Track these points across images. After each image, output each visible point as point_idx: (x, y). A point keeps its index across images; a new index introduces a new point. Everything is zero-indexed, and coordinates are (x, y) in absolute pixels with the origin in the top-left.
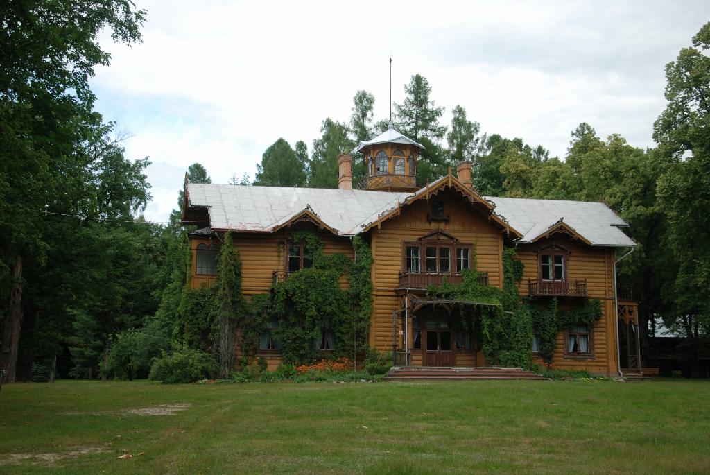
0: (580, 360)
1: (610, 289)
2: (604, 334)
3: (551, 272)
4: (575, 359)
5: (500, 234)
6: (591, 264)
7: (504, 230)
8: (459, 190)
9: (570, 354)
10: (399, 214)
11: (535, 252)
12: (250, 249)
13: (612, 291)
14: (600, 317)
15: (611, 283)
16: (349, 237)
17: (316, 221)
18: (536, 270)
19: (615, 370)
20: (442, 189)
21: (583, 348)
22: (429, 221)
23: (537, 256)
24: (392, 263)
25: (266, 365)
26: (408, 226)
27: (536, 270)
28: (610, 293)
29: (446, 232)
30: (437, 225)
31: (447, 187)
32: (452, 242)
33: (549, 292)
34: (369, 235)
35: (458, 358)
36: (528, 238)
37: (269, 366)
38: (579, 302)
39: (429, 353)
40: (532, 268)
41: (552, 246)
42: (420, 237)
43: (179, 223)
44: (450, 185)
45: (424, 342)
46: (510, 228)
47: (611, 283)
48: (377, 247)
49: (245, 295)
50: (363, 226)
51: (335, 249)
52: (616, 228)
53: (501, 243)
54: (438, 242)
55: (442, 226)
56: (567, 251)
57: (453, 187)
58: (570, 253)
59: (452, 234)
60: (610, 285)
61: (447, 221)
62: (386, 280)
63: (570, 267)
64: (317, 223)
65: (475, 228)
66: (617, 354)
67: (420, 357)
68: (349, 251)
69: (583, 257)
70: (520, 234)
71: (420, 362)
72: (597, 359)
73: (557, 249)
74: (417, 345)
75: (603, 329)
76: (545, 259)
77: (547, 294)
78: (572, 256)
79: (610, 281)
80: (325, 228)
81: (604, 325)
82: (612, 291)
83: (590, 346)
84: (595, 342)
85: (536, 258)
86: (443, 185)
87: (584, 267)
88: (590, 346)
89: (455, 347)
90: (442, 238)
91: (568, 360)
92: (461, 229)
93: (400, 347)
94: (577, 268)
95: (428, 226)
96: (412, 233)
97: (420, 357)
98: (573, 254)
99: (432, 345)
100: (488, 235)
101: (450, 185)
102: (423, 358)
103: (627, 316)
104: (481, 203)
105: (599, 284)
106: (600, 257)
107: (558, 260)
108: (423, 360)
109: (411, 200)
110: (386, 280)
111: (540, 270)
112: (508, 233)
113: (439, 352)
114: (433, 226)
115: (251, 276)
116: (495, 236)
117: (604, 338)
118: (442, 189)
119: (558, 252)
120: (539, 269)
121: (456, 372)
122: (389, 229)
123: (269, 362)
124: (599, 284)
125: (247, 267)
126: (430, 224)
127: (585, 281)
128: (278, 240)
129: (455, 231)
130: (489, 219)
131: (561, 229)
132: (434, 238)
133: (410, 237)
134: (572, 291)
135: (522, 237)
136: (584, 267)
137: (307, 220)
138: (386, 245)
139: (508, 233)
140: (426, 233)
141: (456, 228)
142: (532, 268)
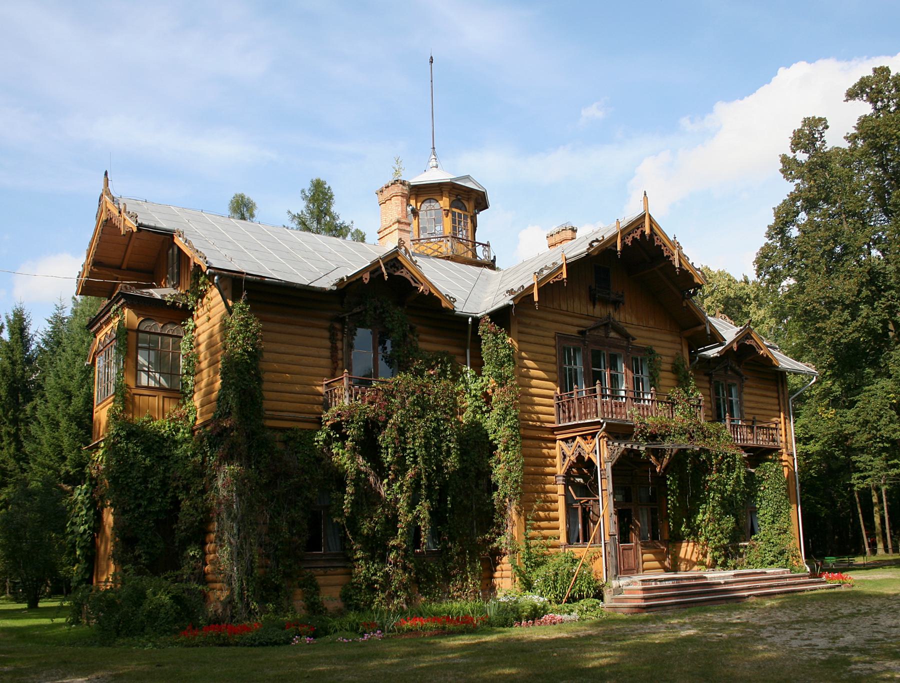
7: (700, 328)
10: (565, 276)
11: (706, 375)
14: (128, 422)
23: (710, 382)
25: (317, 588)
37: (322, 589)
41: (726, 367)
42: (581, 329)
43: (144, 564)
49: (271, 428)
61: (616, 304)
63: (746, 404)
65: (651, 323)
69: (767, 390)
87: (760, 405)
90: (613, 334)
96: (569, 320)
100: (669, 338)
114: (599, 311)
116: (678, 340)
121: (720, 584)
123: (320, 580)
125: (272, 376)
132: (601, 333)
133: (565, 327)
136: (760, 405)
138: (532, 339)
140: (589, 323)
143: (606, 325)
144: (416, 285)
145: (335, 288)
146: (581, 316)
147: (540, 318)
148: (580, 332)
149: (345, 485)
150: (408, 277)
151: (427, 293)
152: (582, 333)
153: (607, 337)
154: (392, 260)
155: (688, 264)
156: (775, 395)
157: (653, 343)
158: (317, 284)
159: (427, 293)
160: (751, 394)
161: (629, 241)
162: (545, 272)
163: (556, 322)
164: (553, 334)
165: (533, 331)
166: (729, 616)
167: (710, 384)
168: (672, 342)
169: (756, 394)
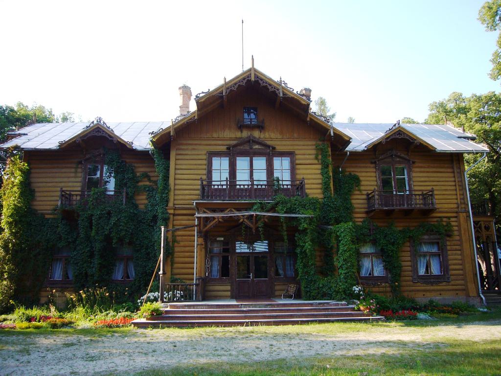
1: (462, 201)
4: (427, 283)
6: (439, 175)
8: (273, 90)
11: (372, 163)
13: (464, 203)
15: (463, 195)
16: (148, 151)
17: (109, 135)
18: (375, 183)
19: (476, 295)
23: (375, 167)
26: (215, 135)
27: (375, 183)
28: (463, 206)
32: (268, 150)
34: (166, 142)
35: (277, 288)
36: (359, 142)
40: (369, 179)
41: (392, 156)
44: (253, 79)
46: (334, 129)
48: (177, 154)
50: (152, 133)
55: (256, 134)
56: (409, 160)
58: (414, 163)
59: (269, 143)
60: (462, 197)
63: (414, 179)
66: (476, 274)
67: (229, 288)
69: (428, 167)
70: (347, 136)
71: (229, 293)
72: (453, 283)
78: (417, 167)
79: (461, 193)
82: (464, 203)
84: (450, 262)
85: (374, 170)
86: (244, 79)
90: (257, 147)
91: (419, 284)
92: (279, 136)
94: (422, 179)
95: (239, 134)
98: (417, 165)
101: (253, 79)
103: (484, 233)
106: (448, 168)
108: (232, 291)
109: (202, 97)
112: (332, 134)
114: (245, 134)
115: (49, 194)
119: (399, 163)
122: (200, 139)
126: (242, 132)
127: (432, 191)
129: (272, 139)
131: (399, 134)
132: (247, 147)
134: (418, 203)
139: (332, 134)
140: (235, 142)
141: (273, 135)
142: (369, 179)
143: (249, 141)
144: (111, 139)
145: (366, 149)
147: (196, 144)
153: (251, 149)
155: (294, 94)
160: (417, 172)
163: (210, 145)
164: (205, 152)
165: (189, 153)
169: (427, 172)
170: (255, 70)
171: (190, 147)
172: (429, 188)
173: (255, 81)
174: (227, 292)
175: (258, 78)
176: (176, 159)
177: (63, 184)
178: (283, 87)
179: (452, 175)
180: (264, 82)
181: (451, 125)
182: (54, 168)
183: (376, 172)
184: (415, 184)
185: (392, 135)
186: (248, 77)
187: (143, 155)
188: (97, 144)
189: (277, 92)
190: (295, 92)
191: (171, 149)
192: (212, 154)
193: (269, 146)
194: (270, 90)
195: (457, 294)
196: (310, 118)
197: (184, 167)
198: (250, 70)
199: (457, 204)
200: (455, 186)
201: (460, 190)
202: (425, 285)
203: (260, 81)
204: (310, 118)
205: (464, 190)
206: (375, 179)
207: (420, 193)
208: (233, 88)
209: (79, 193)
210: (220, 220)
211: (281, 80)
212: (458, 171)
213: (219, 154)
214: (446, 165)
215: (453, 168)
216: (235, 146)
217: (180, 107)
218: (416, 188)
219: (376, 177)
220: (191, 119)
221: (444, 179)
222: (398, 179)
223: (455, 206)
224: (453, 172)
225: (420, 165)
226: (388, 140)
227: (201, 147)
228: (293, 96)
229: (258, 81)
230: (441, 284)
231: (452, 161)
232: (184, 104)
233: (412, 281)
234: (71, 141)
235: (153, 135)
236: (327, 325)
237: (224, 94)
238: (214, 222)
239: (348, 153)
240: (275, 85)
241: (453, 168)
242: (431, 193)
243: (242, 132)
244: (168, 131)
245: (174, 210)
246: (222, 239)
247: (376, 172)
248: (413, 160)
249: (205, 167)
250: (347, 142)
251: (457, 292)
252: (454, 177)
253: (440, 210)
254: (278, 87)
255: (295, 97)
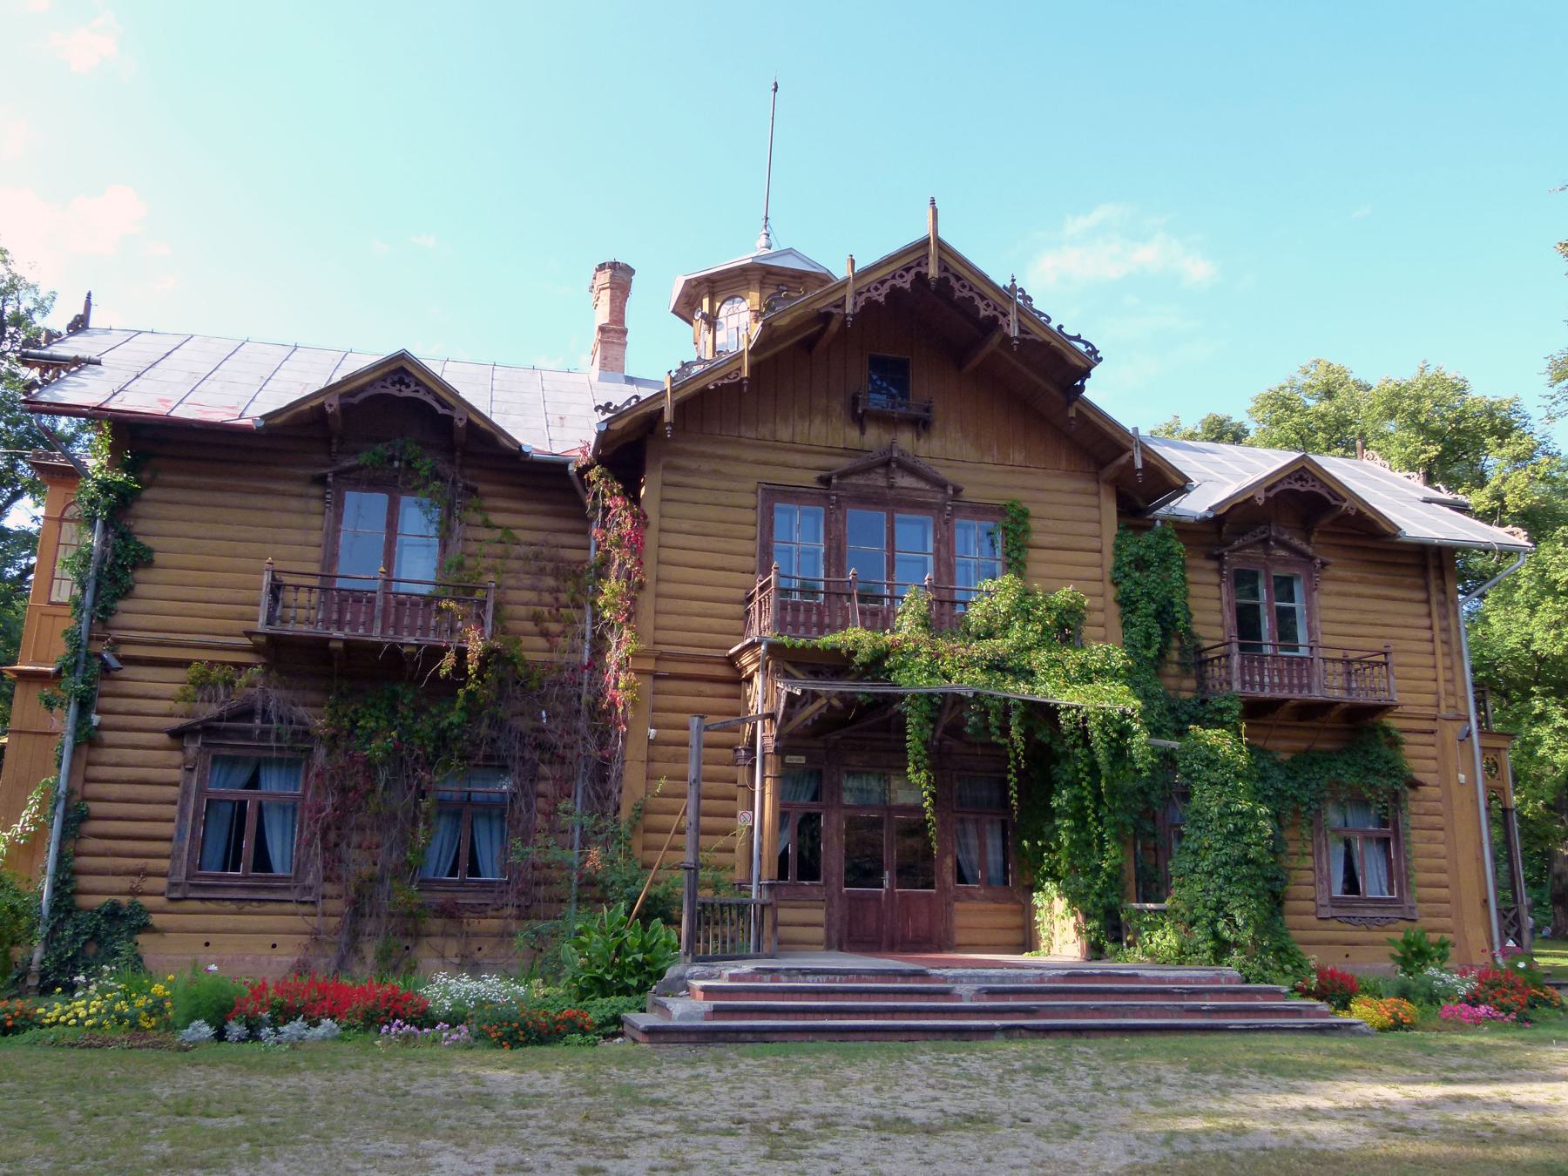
0: (1368, 924)
2: (1440, 834)
3: (1266, 625)
5: (1105, 481)
7: (1124, 459)
8: (966, 293)
9: (1334, 902)
10: (746, 374)
11: (1210, 557)
12: (196, 496)
15: (1451, 668)
16: (565, 465)
17: (439, 400)
20: (906, 283)
21: (1373, 881)
22: (859, 420)
23: (1219, 571)
24: (718, 560)
26: (784, 434)
27: (1218, 618)
29: (924, 463)
30: (887, 438)
31: (921, 278)
33: (1272, 686)
38: (1359, 728)
39: (851, 898)
41: (1265, 541)
42: (823, 473)
44: (933, 271)
45: (833, 856)
46: (1146, 450)
47: (1451, 668)
50: (606, 408)
51: (529, 513)
52: (1446, 510)
53: (1110, 508)
54: (890, 494)
55: (905, 440)
56: (1312, 559)
57: (943, 282)
58: (1324, 564)
59: (945, 474)
61: (921, 425)
62: (697, 622)
64: (444, 404)
65: (1018, 457)
67: (819, 915)
68: (572, 524)
69: (1361, 581)
71: (820, 933)
73: (1282, 553)
74: (798, 864)
75: (1436, 819)
76: (1244, 580)
77: (1267, 693)
80: (469, 421)
81: (1437, 792)
83: (1396, 874)
85: (1215, 579)
87: (1370, 617)
88: (1396, 874)
89: (949, 878)
90: (904, 481)
91: (1334, 923)
92: (970, 453)
93: (739, 875)
94: (1345, 616)
95: (852, 436)
97: (819, 915)
99: (863, 871)
101: (933, 271)
102: (828, 915)
104: (1045, 344)
105: (1416, 673)
107: (1284, 588)
108: (829, 926)
110: (697, 622)
111: (1230, 620)
112: (1139, 465)
113: (890, 893)
114: (874, 438)
116: (1092, 486)
117: (1442, 849)
118: (906, 283)
119: (1286, 562)
120: (1228, 615)
124: (1416, 673)
126: (863, 432)
128: (310, 471)
130: (1072, 413)
131: (1301, 478)
134: (1329, 687)
135: (1181, 485)
137: (407, 393)
138: (699, 496)
139: (1139, 465)
140: (843, 463)
143: (886, 464)
144: (446, 412)
145: (1211, 515)
146: (830, 451)
147: (723, 458)
148: (821, 480)
149: (933, 805)
150: (1323, 492)
151: (1353, 513)
152: (825, 481)
153: (891, 487)
154: (395, 372)
155: (1049, 331)
156: (1421, 595)
157: (1018, 495)
158: (183, 413)
159: (1353, 513)
161: (861, 301)
162: (696, 369)
163: (765, 463)
164: (752, 485)
166: (837, 1087)
167: (1221, 575)
168: (1074, 492)
169: (1358, 596)
170: (941, 246)
171: (705, 466)
172: (1379, 645)
173: (940, 279)
174: (813, 929)
175: (946, 269)
176: (663, 500)
177: (281, 550)
178: (1020, 309)
179: (1423, 609)
180: (964, 286)
181: (1379, 460)
182: (220, 489)
183: (1219, 586)
184: (1327, 627)
185: (1281, 481)
186: (919, 265)
187: (548, 481)
188: (392, 427)
189: (1002, 321)
190: (1054, 325)
191: (649, 464)
192: (775, 493)
193: (941, 485)
194: (983, 313)
195: (207, 944)
196: (1078, 411)
197: (686, 526)
198: (925, 243)
199: (1436, 693)
200: (1432, 641)
201: (1444, 655)
202: (1349, 926)
203: (953, 281)
204: (1078, 411)
205: (1456, 657)
206: (1216, 605)
207: (1339, 655)
208: (874, 295)
209: (315, 582)
210: (835, 702)
211: (1013, 286)
212: (1441, 597)
213: (792, 494)
214: (1409, 580)
215: (1426, 588)
216: (843, 475)
217: (602, 329)
218: (1327, 640)
219: (1220, 599)
220: (726, 377)
221: (1400, 620)
222: (1278, 608)
223: (1430, 699)
224: (1428, 601)
225: (1340, 573)
226: (1271, 494)
227: (741, 469)
228: (1048, 338)
229: (946, 280)
230: (1392, 926)
231: (1424, 570)
232: (613, 321)
233: (1316, 913)
234: (306, 407)
235: (608, 415)
236: (1260, 1040)
237: (849, 309)
238: (816, 705)
239: (1158, 523)
240: (998, 300)
241: (1426, 588)
242: (1381, 658)
243: (863, 432)
244: (656, 407)
245: (657, 659)
246: (802, 760)
247: (1219, 586)
248: (1325, 559)
249: (751, 531)
250: (1172, 483)
251: (276, 938)
252: (1429, 615)
253: (1406, 709)
254: (1004, 304)
255: (1054, 343)
